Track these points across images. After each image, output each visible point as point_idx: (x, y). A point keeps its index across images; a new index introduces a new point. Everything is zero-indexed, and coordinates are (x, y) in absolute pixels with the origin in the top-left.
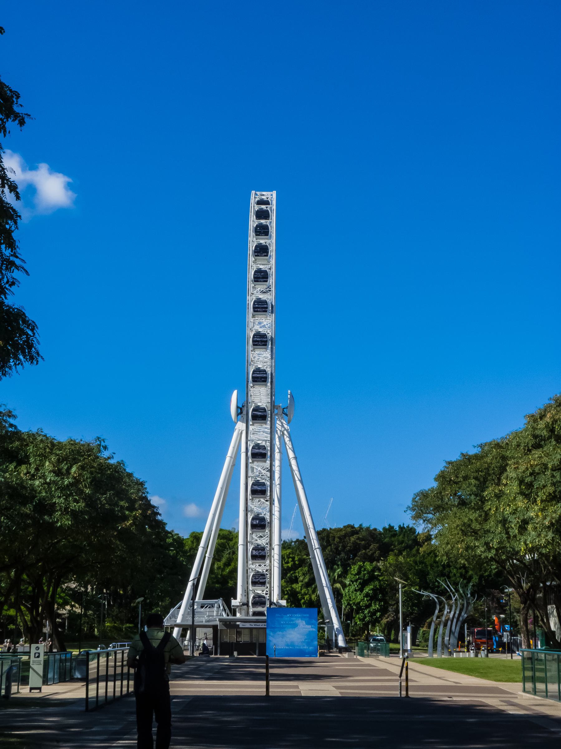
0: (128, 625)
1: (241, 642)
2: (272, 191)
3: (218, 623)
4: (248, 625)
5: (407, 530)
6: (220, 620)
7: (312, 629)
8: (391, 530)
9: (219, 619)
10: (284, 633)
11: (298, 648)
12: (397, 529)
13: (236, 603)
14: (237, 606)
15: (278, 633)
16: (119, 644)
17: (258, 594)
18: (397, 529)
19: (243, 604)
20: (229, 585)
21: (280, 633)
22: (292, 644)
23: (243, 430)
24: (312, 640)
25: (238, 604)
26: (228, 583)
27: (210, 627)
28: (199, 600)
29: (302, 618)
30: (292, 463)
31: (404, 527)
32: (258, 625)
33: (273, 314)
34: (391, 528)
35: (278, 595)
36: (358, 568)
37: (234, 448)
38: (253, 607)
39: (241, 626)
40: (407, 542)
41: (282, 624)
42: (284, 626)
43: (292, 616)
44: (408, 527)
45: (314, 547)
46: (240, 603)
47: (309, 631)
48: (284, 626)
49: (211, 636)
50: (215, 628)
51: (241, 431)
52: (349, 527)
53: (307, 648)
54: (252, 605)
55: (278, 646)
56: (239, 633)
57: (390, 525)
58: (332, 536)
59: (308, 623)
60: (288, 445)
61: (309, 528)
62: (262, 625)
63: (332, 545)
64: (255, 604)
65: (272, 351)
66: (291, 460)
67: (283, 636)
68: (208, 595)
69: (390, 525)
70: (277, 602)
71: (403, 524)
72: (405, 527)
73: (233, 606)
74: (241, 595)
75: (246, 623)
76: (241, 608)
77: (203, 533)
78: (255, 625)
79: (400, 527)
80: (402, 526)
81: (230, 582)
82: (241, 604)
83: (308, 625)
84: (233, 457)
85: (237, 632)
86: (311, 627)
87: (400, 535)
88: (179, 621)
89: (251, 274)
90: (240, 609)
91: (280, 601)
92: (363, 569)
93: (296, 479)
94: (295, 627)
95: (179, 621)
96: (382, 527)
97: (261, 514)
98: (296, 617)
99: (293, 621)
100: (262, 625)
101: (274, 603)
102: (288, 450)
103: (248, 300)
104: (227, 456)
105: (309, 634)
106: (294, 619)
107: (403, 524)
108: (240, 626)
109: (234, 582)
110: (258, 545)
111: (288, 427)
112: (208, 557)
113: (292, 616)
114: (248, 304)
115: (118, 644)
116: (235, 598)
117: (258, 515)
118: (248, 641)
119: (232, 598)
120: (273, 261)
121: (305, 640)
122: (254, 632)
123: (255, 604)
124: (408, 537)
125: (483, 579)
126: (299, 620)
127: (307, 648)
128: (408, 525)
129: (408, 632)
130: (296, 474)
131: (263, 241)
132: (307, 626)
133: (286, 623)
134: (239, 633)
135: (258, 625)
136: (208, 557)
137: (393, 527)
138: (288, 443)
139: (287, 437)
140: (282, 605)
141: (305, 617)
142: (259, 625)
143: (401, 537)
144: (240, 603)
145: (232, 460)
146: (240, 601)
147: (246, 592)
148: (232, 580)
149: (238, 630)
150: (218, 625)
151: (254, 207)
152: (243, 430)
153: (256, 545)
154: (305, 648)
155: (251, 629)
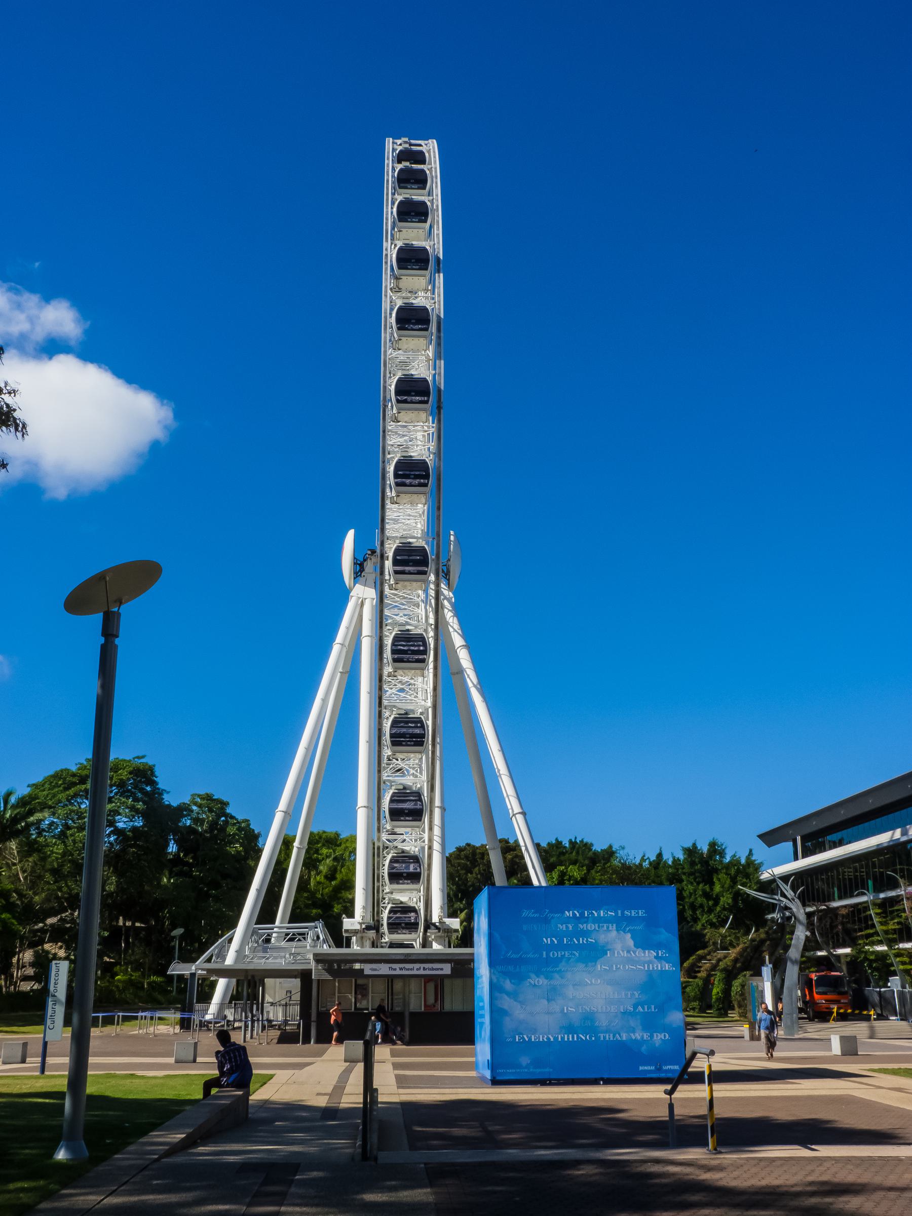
0: (154, 978)
1: (367, 1009)
2: (428, 140)
3: (313, 965)
4: (384, 969)
5: (581, 846)
6: (319, 958)
7: (658, 966)
8: (559, 846)
9: (315, 955)
10: (557, 981)
11: (609, 1037)
12: (567, 845)
13: (352, 924)
14: (355, 932)
15: (534, 980)
16: (121, 1014)
17: (402, 903)
18: (567, 845)
19: (368, 928)
20: (336, 910)
21: (542, 981)
22: (588, 1022)
23: (366, 599)
24: (662, 1009)
25: (358, 927)
26: (333, 907)
27: (295, 977)
28: (281, 924)
29: (621, 923)
30: (460, 657)
31: (576, 842)
32: (408, 969)
33: (442, 275)
34: (559, 844)
35: (442, 908)
36: (559, 876)
37: (348, 628)
38: (390, 933)
39: (367, 972)
40: (583, 861)
41: (552, 947)
42: (554, 954)
43: (582, 914)
44: (582, 841)
45: (510, 811)
46: (361, 924)
47: (650, 974)
48: (554, 954)
49: (297, 997)
50: (305, 976)
51: (362, 601)
52: (503, 841)
53: (646, 1036)
54: (388, 929)
55: (534, 1033)
56: (361, 990)
57: (557, 839)
58: (480, 853)
59: (643, 943)
60: (451, 624)
61: (500, 775)
62: (417, 969)
63: (481, 866)
64: (394, 926)
65: (438, 344)
66: (458, 651)
67: (552, 994)
68: (296, 916)
69: (557, 839)
70: (440, 922)
71: (576, 838)
72: (578, 842)
73: (347, 931)
74: (364, 908)
75: (379, 965)
76: (364, 935)
77: (295, 836)
78: (401, 969)
79: (570, 842)
80: (573, 841)
81: (336, 905)
82: (364, 926)
83: (644, 949)
84: (347, 644)
85: (357, 986)
86: (657, 957)
87: (571, 853)
88: (230, 960)
89: (391, 252)
90: (362, 938)
91: (448, 921)
92: (567, 877)
93: (470, 685)
94: (595, 959)
95: (230, 960)
96: (546, 843)
97: (413, 711)
98: (599, 920)
99: (586, 934)
100: (417, 969)
101: (434, 925)
102: (452, 633)
103: (386, 250)
104: (336, 642)
105: (650, 983)
106: (591, 926)
107: (576, 838)
108: (366, 973)
109: (342, 906)
110: (405, 788)
111: (450, 593)
112: (298, 848)
113: (582, 914)
114: (387, 255)
115: (119, 1016)
116: (351, 915)
117: (406, 714)
118: (445, 1008)
119: (344, 916)
120: (438, 231)
121: (635, 1006)
122: (398, 985)
123: (394, 926)
124: (582, 855)
125: (740, 898)
126: (608, 930)
127: (646, 1036)
128: (582, 840)
129: (765, 979)
130: (468, 676)
131: (417, 196)
132: (639, 952)
133: (560, 941)
134: (361, 990)
135: (408, 969)
136: (298, 848)
137: (561, 843)
138: (451, 621)
139: (449, 610)
140: (452, 929)
141: (630, 920)
142: (411, 969)
143: (574, 854)
144: (361, 924)
145: (345, 650)
146: (361, 921)
147: (375, 903)
148: (338, 904)
149: (361, 981)
150: (312, 969)
151: (391, 169)
152: (366, 599)
153: (401, 787)
154: (637, 1036)
155: (390, 979)
